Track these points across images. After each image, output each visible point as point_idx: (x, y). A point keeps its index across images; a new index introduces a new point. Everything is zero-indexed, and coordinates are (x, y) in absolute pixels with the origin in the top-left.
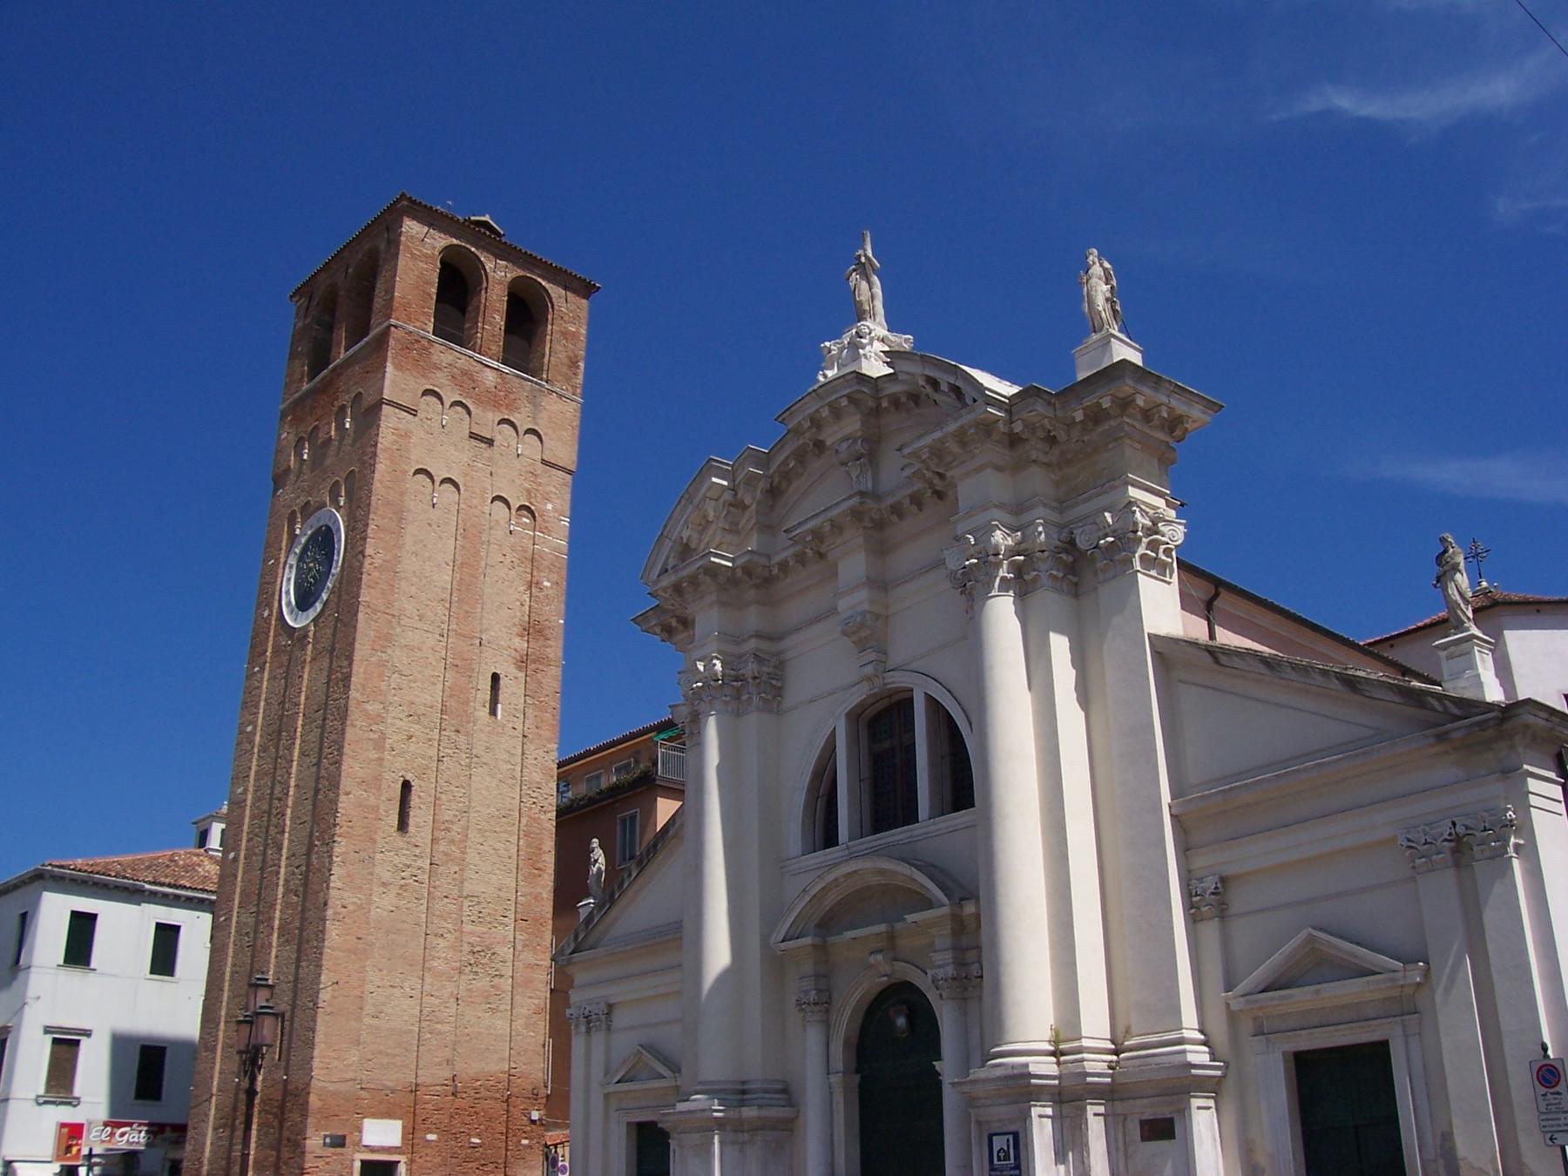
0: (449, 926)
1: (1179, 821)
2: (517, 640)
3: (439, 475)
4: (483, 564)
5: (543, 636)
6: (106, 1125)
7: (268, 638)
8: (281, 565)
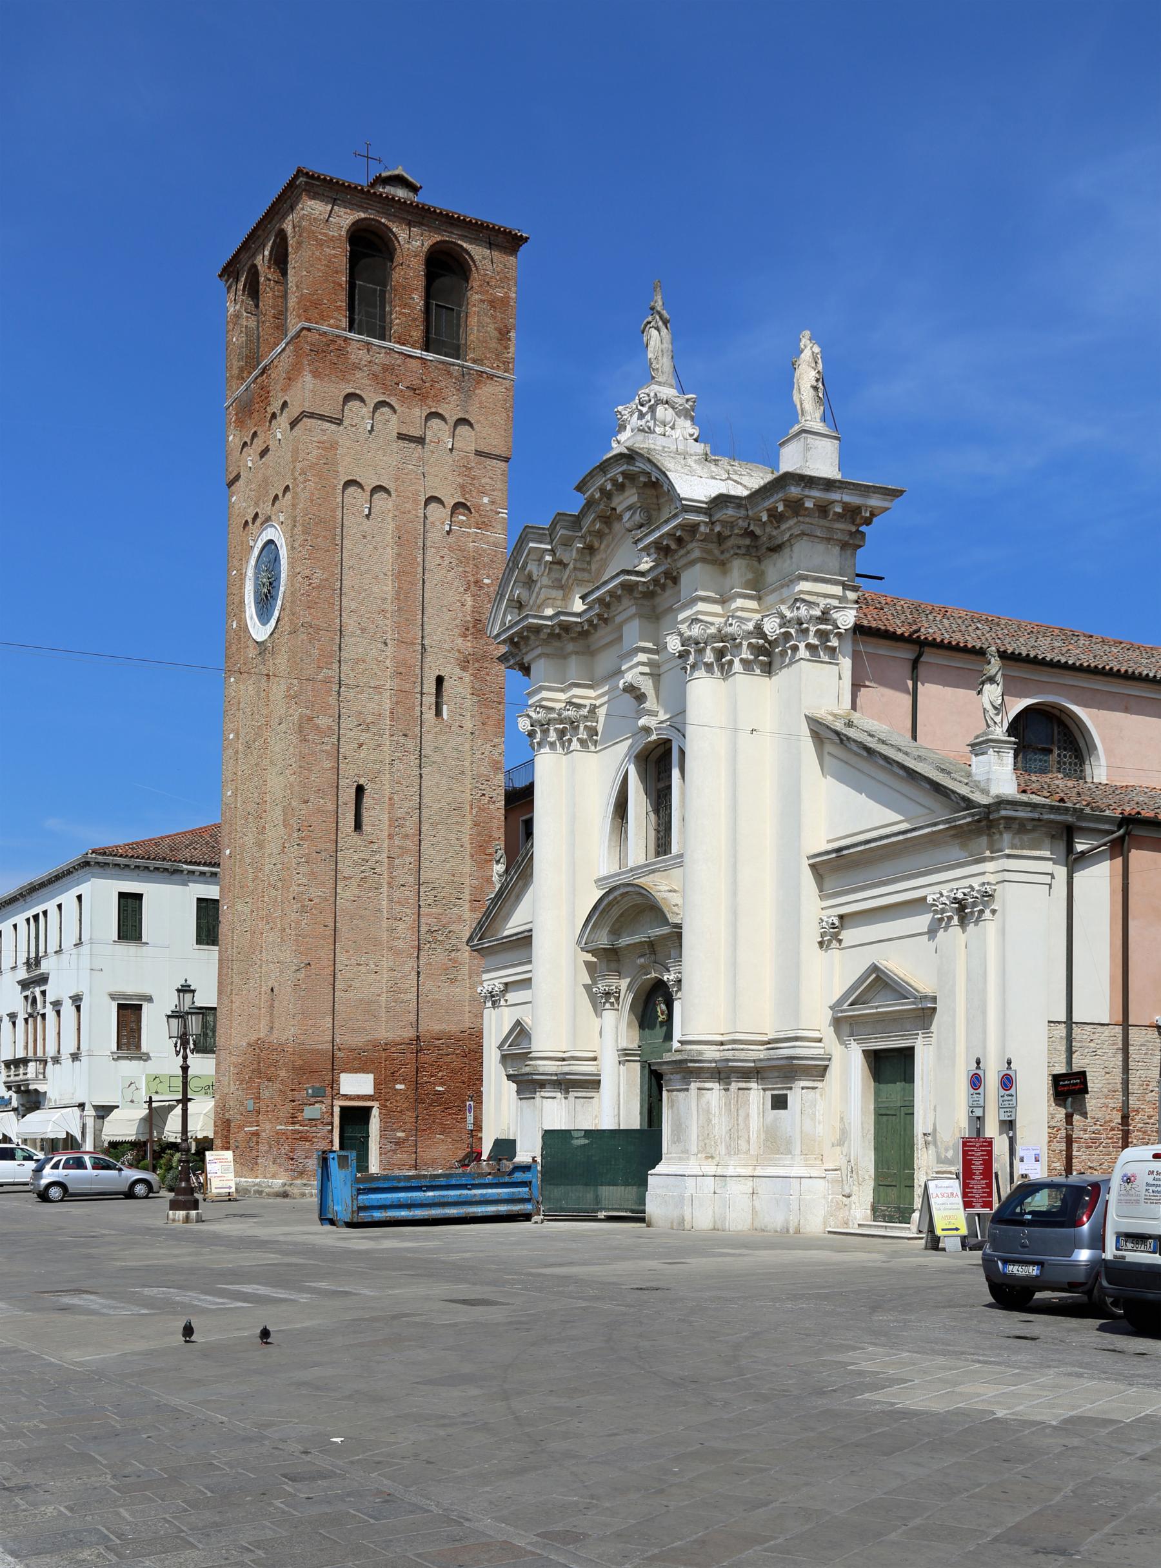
1: (817, 869)
2: (460, 641)
3: (369, 483)
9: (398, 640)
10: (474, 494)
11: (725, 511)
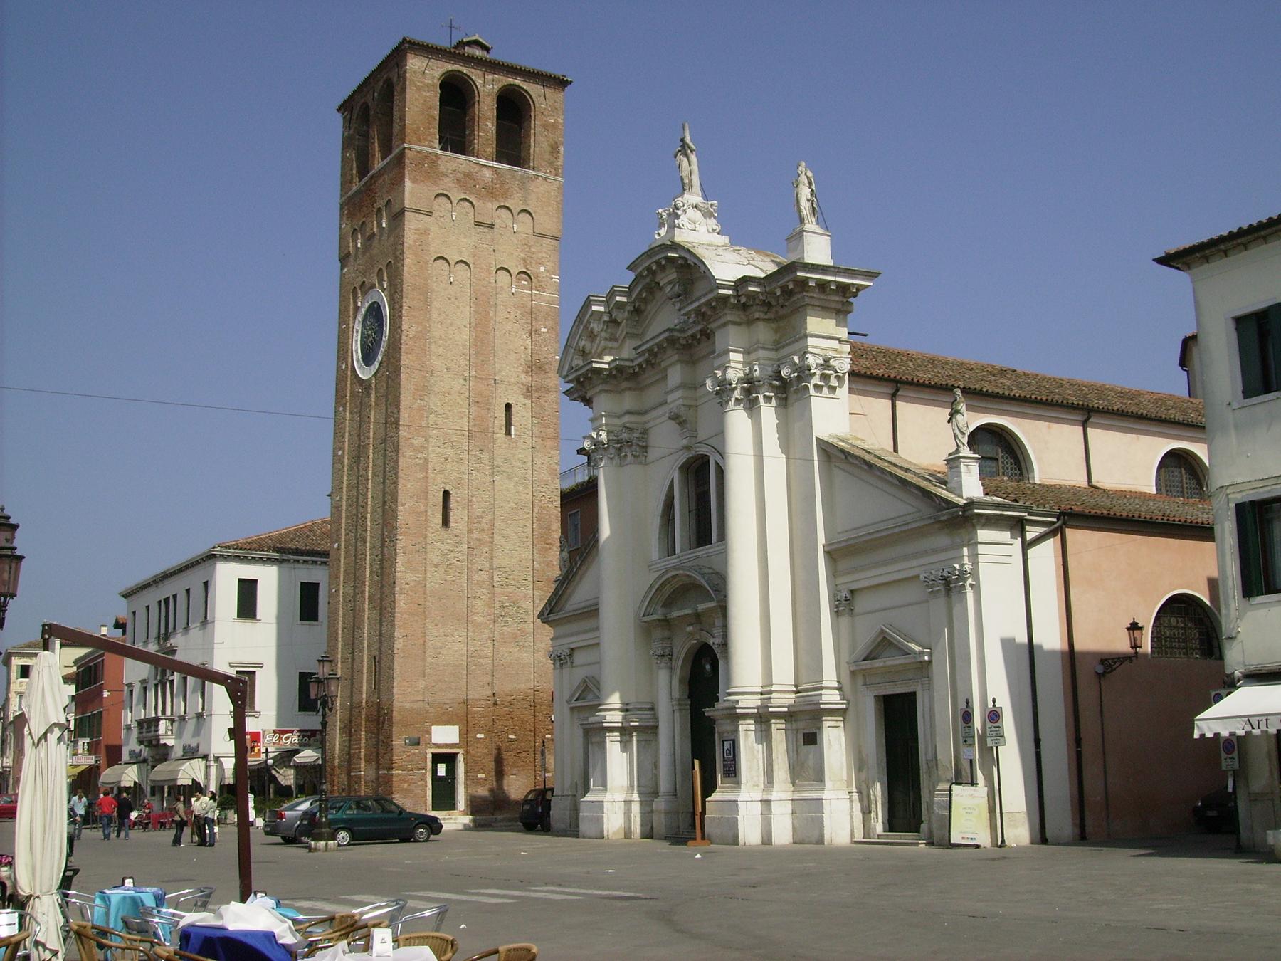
0: (484, 590)
1: (831, 555)
2: (523, 376)
3: (453, 258)
4: (492, 322)
5: (543, 370)
6: (275, 732)
7: (346, 385)
8: (351, 329)
9: (476, 376)
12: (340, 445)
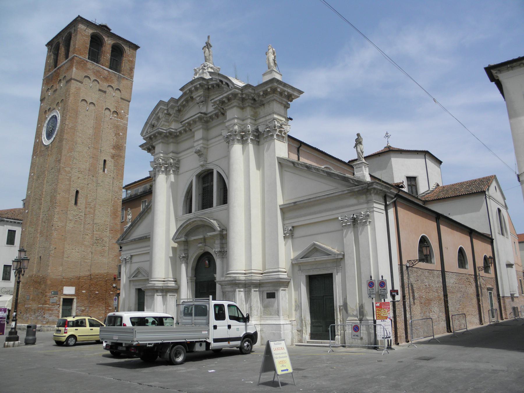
0: (90, 232)
2: (112, 150)
3: (89, 101)
10: (119, 109)
11: (248, 90)
12: (33, 171)
